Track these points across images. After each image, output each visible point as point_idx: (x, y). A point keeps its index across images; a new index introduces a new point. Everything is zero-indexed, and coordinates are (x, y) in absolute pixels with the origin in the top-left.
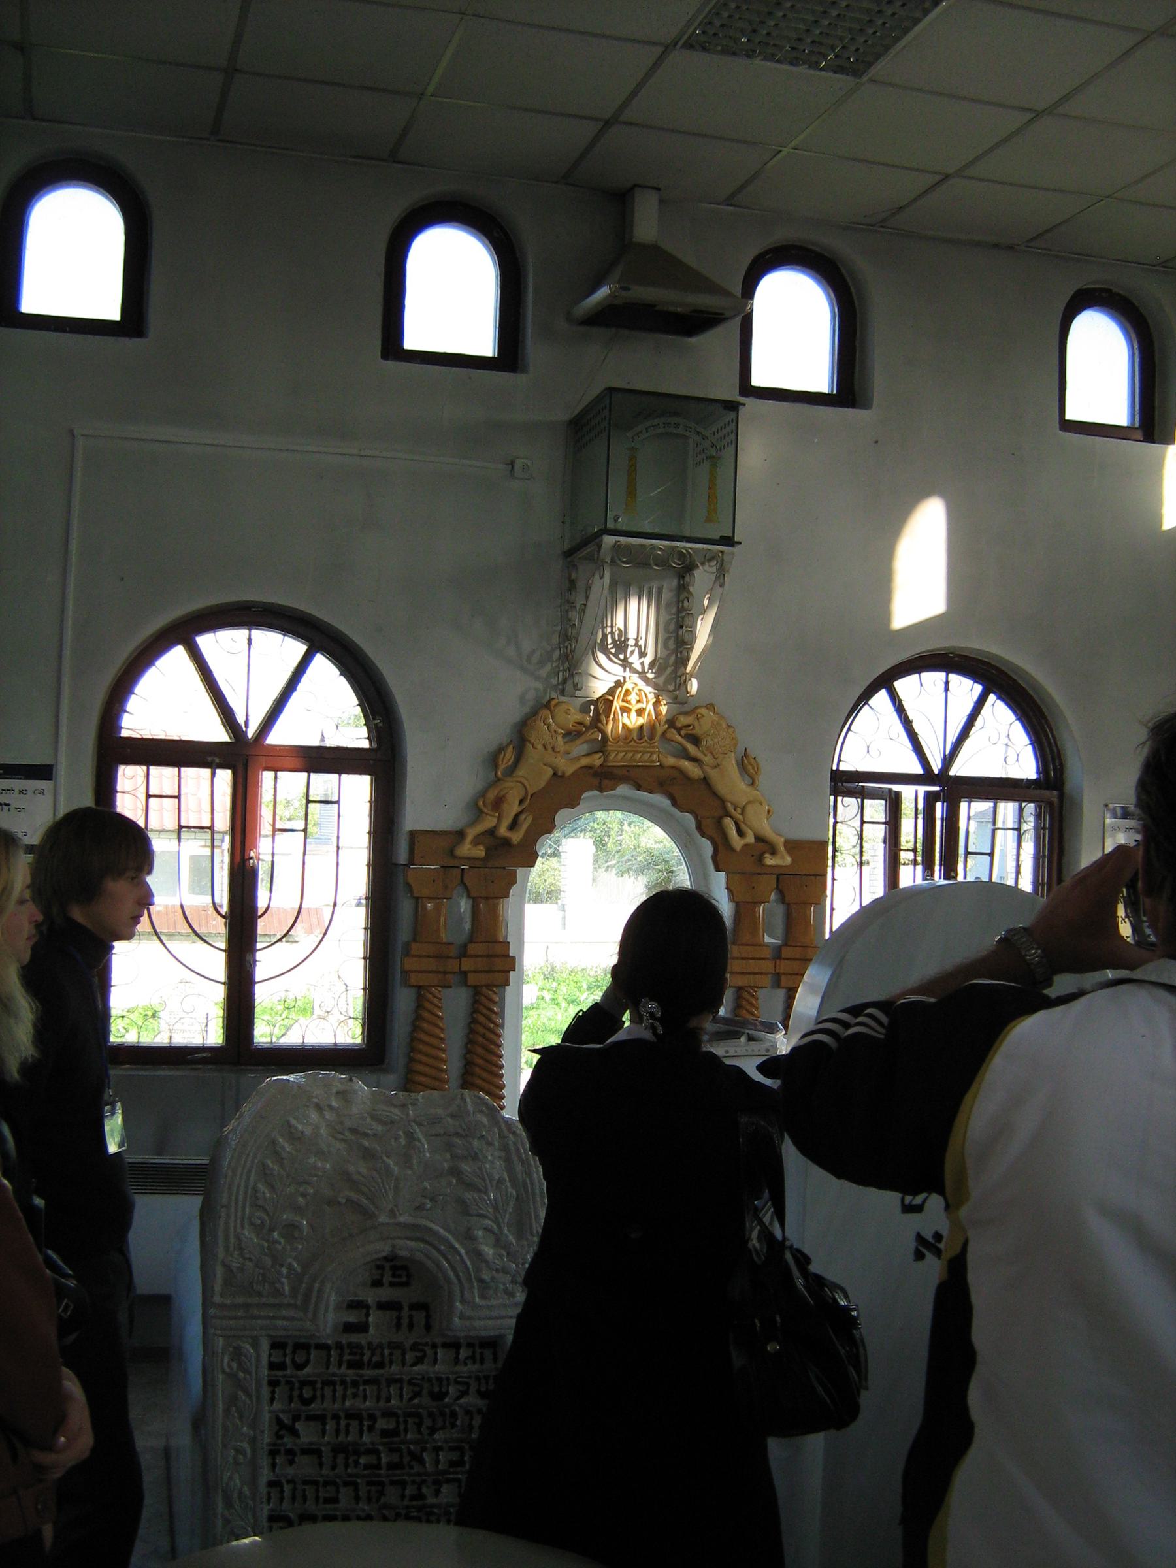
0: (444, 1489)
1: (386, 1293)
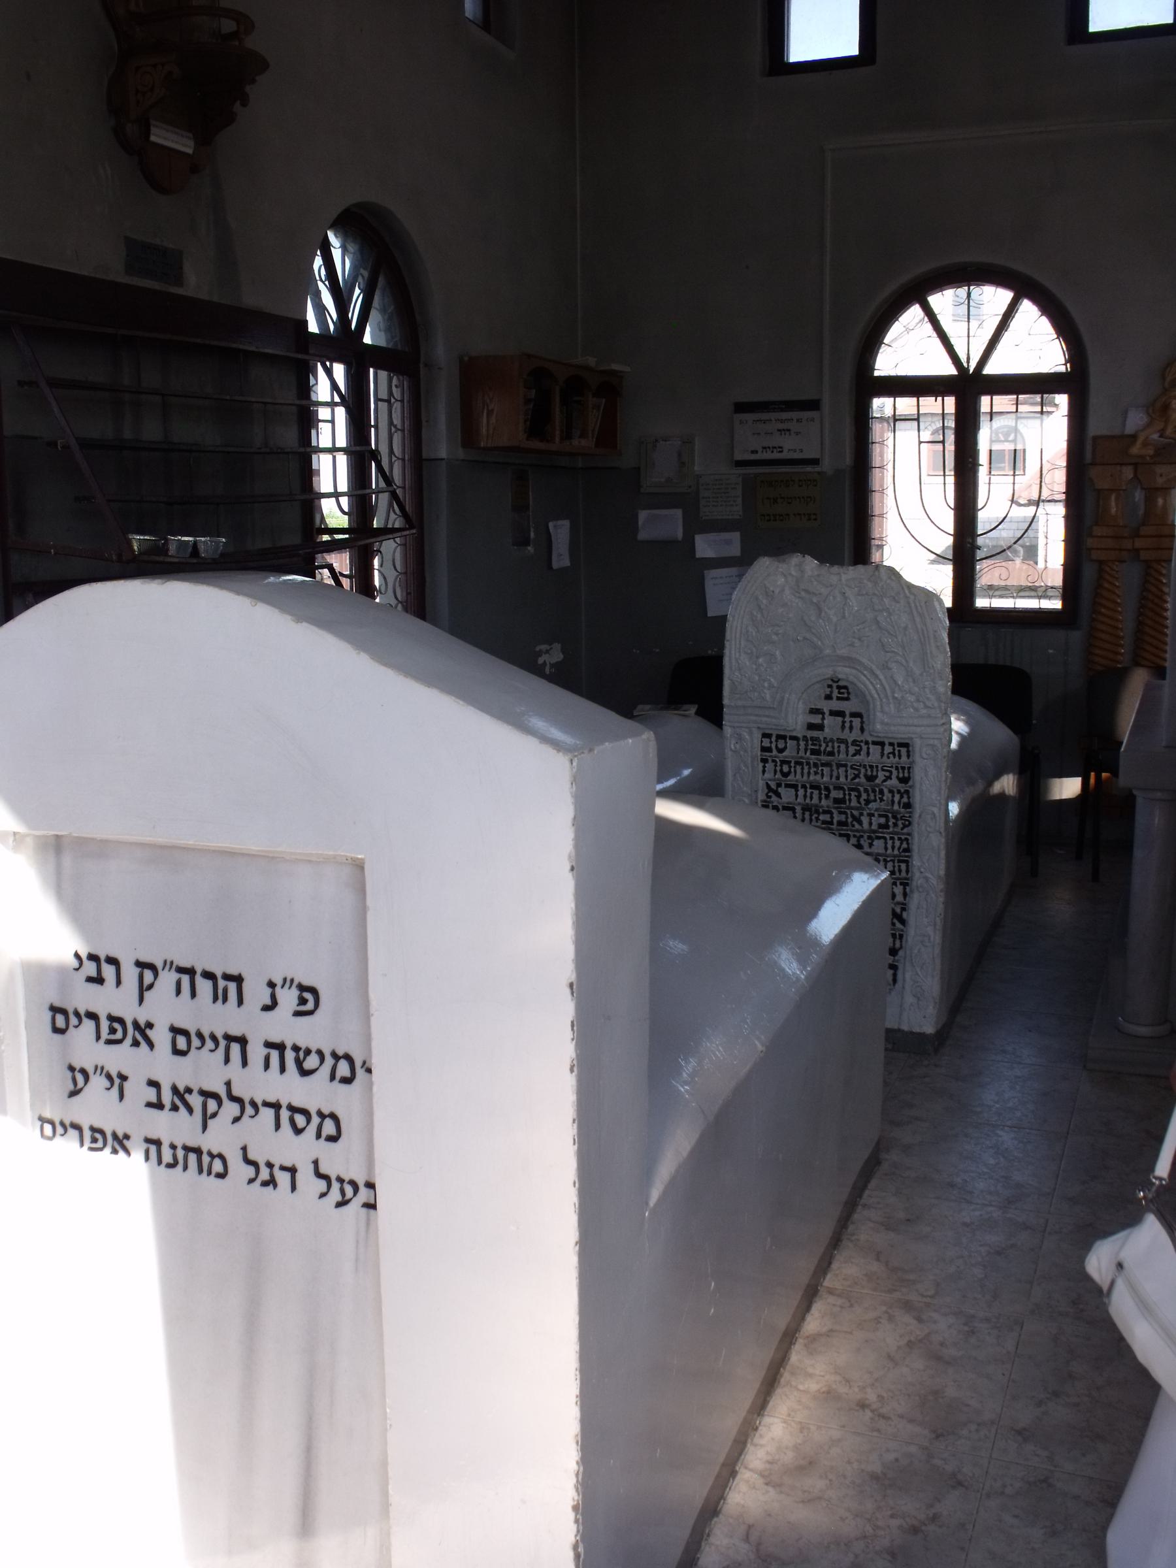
0: (876, 842)
1: (835, 705)
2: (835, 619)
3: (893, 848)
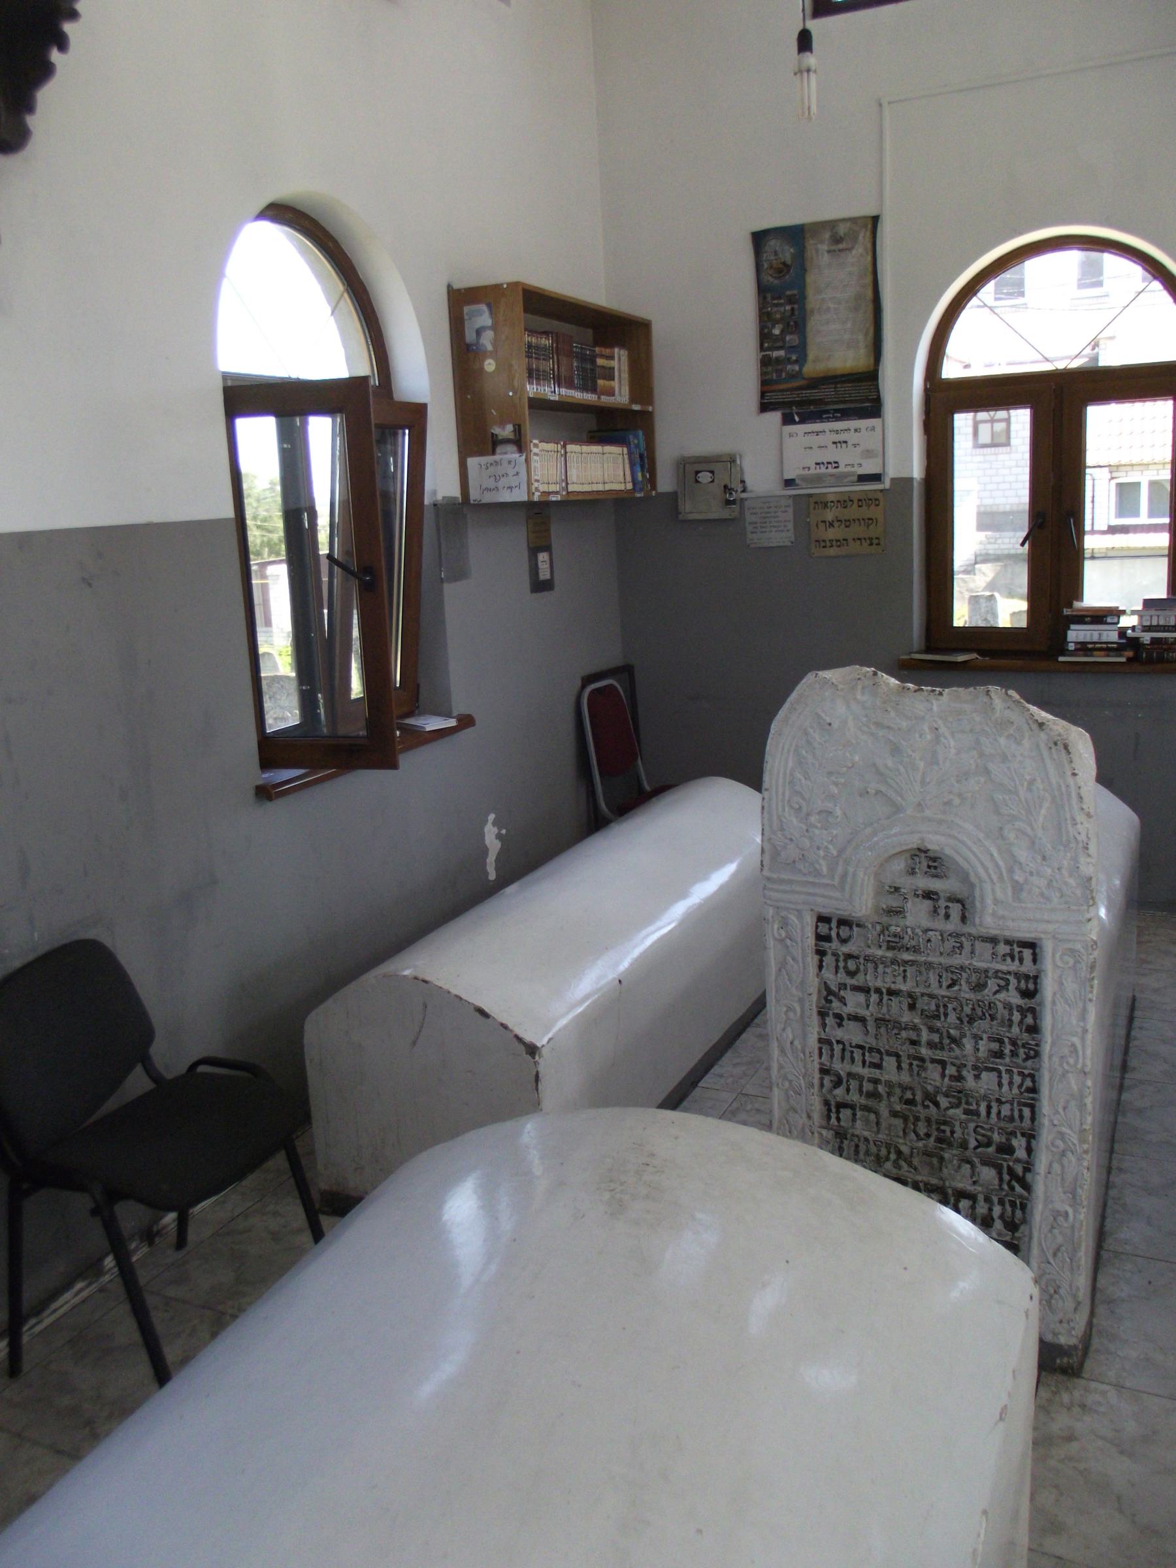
0: (984, 1075)
2: (921, 764)
3: (1011, 1083)
